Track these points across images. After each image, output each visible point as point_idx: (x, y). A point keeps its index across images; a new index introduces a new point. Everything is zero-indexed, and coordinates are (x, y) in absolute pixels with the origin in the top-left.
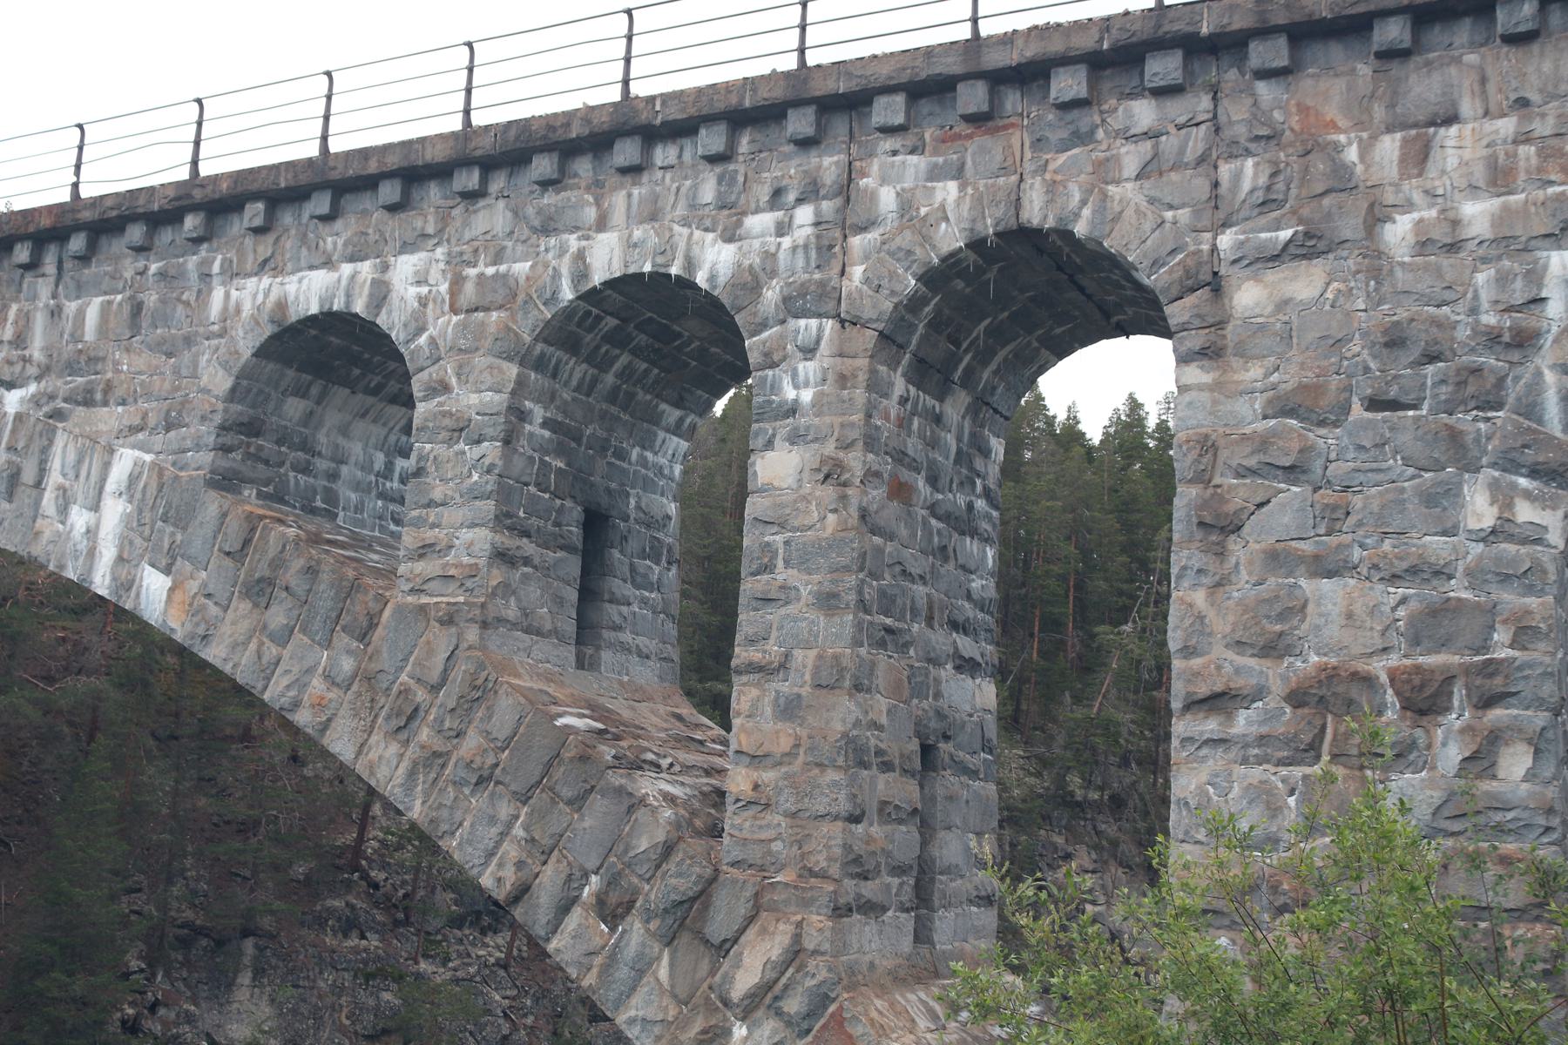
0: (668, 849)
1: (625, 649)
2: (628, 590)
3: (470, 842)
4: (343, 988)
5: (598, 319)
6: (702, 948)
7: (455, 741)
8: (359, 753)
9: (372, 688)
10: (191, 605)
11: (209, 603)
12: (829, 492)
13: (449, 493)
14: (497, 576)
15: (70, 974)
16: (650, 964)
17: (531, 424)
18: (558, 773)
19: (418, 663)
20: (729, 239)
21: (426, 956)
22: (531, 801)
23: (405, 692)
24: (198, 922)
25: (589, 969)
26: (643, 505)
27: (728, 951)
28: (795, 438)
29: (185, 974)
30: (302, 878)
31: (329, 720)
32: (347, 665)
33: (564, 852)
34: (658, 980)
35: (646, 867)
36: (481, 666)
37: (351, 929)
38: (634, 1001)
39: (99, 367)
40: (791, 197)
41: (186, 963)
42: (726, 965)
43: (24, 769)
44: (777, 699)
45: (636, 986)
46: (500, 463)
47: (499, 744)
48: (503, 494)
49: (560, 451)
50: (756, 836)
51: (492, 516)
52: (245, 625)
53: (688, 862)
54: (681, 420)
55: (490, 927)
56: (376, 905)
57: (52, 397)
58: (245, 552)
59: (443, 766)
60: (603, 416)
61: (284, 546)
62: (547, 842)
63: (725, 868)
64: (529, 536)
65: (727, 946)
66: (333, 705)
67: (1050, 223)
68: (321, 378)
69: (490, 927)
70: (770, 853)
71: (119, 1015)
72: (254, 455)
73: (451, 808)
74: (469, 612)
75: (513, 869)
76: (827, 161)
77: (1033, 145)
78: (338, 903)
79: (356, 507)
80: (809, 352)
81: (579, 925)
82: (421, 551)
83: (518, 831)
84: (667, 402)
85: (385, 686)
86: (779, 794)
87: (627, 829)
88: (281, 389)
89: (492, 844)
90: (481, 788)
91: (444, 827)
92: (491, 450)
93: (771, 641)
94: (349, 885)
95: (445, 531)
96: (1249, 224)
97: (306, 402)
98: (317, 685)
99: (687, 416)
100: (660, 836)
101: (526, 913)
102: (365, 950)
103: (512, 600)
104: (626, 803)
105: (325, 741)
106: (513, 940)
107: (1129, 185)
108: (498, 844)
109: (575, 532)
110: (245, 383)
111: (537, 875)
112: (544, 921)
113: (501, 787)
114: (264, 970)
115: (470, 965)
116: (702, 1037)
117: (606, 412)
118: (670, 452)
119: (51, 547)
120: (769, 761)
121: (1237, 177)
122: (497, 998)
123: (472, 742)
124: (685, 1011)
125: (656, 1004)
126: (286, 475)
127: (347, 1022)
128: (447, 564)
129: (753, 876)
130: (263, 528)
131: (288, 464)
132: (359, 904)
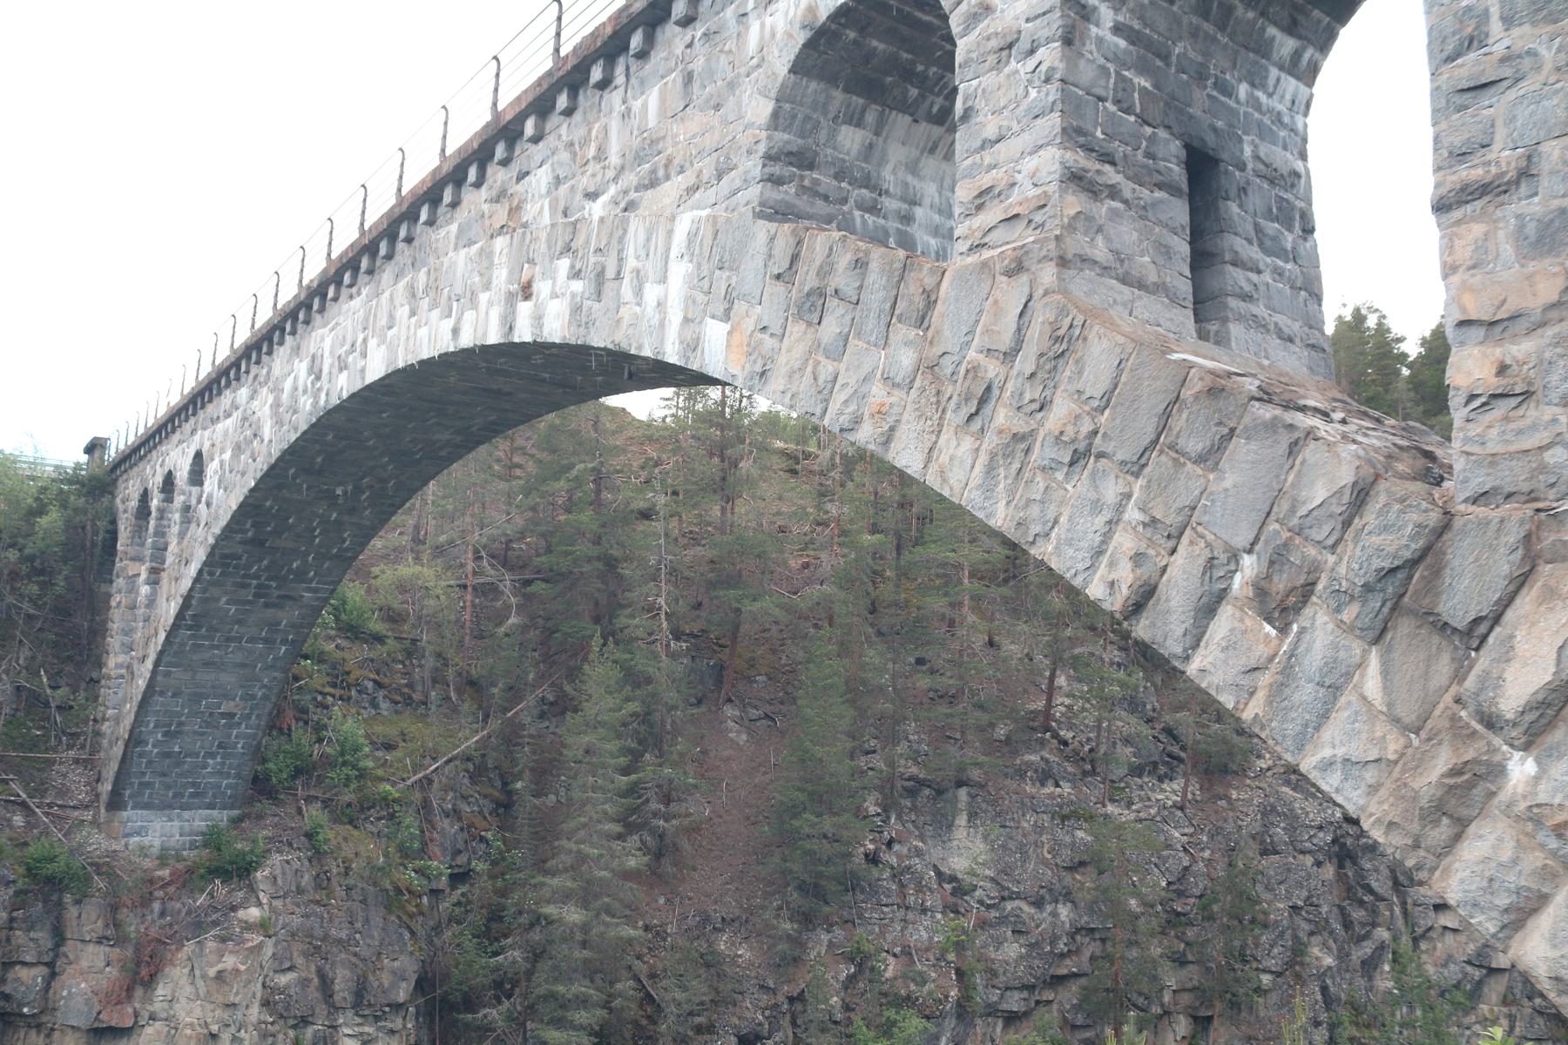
0: (1360, 495)
1: (1262, 326)
2: (1253, 252)
3: (1069, 542)
4: (1043, 828)
6: (1436, 639)
7: (1039, 415)
8: (928, 460)
9: (936, 379)
10: (749, 345)
11: (766, 337)
13: (1005, 123)
14: (1074, 203)
15: (819, 815)
16: (1349, 675)
17: (1097, 25)
18: (1179, 422)
19: (987, 331)
21: (1112, 800)
22: (1147, 470)
23: (974, 370)
24: (921, 776)
25: (1252, 694)
26: (1262, 155)
27: (1484, 638)
29: (913, 817)
30: (1003, 738)
31: (892, 429)
32: (906, 359)
33: (1200, 529)
34: (1364, 698)
35: (1327, 529)
36: (1062, 311)
37: (1046, 779)
38: (1327, 733)
39: (661, 146)
41: (914, 808)
42: (1483, 661)
43: (783, 662)
44: (1521, 228)
45: (1328, 711)
46: (1061, 66)
47: (1096, 403)
48: (1071, 104)
49: (1143, 69)
50: (1513, 448)
51: (1058, 129)
52: (799, 351)
53: (1397, 507)
54: (1297, 55)
55: (1166, 775)
56: (1067, 758)
57: (626, 192)
58: (794, 269)
59: (1027, 451)
60: (1194, 34)
61: (831, 249)
62: (1173, 519)
63: (1462, 507)
64: (1113, 163)
65: (1482, 629)
66: (895, 410)
68: (875, 102)
69: (1166, 775)
70: (1543, 468)
71: (862, 849)
72: (809, 189)
73: (1042, 502)
74: (1041, 249)
75: (1129, 565)
78: (1034, 758)
79: (937, 253)
81: (1232, 630)
82: (978, 201)
83: (1132, 514)
84: (1276, 24)
85: (949, 371)
86: (1547, 372)
87: (1291, 478)
88: (831, 116)
89: (1098, 539)
90: (1077, 468)
91: (1035, 529)
92: (1050, 55)
93: (1496, 147)
94: (1042, 742)
95: (1004, 169)
97: (863, 132)
98: (878, 392)
99: (1304, 49)
100: (1346, 476)
101: (1153, 625)
102: (1060, 796)
103: (1100, 239)
104: (1285, 439)
105: (890, 456)
106: (1186, 785)
108: (1107, 537)
109: (1178, 173)
110: (787, 106)
111: (1164, 570)
112: (1180, 631)
113: (1104, 460)
114: (976, 813)
115: (1150, 807)
116: (1452, 781)
117: (1198, 28)
118: (1288, 97)
119: (630, 331)
120: (1522, 325)
122: (1177, 835)
123: (1061, 409)
124: (1416, 742)
125: (1364, 736)
126: (850, 212)
127: (1049, 856)
128: (1010, 205)
129: (1516, 509)
130: (810, 239)
131: (851, 202)
132: (1052, 758)
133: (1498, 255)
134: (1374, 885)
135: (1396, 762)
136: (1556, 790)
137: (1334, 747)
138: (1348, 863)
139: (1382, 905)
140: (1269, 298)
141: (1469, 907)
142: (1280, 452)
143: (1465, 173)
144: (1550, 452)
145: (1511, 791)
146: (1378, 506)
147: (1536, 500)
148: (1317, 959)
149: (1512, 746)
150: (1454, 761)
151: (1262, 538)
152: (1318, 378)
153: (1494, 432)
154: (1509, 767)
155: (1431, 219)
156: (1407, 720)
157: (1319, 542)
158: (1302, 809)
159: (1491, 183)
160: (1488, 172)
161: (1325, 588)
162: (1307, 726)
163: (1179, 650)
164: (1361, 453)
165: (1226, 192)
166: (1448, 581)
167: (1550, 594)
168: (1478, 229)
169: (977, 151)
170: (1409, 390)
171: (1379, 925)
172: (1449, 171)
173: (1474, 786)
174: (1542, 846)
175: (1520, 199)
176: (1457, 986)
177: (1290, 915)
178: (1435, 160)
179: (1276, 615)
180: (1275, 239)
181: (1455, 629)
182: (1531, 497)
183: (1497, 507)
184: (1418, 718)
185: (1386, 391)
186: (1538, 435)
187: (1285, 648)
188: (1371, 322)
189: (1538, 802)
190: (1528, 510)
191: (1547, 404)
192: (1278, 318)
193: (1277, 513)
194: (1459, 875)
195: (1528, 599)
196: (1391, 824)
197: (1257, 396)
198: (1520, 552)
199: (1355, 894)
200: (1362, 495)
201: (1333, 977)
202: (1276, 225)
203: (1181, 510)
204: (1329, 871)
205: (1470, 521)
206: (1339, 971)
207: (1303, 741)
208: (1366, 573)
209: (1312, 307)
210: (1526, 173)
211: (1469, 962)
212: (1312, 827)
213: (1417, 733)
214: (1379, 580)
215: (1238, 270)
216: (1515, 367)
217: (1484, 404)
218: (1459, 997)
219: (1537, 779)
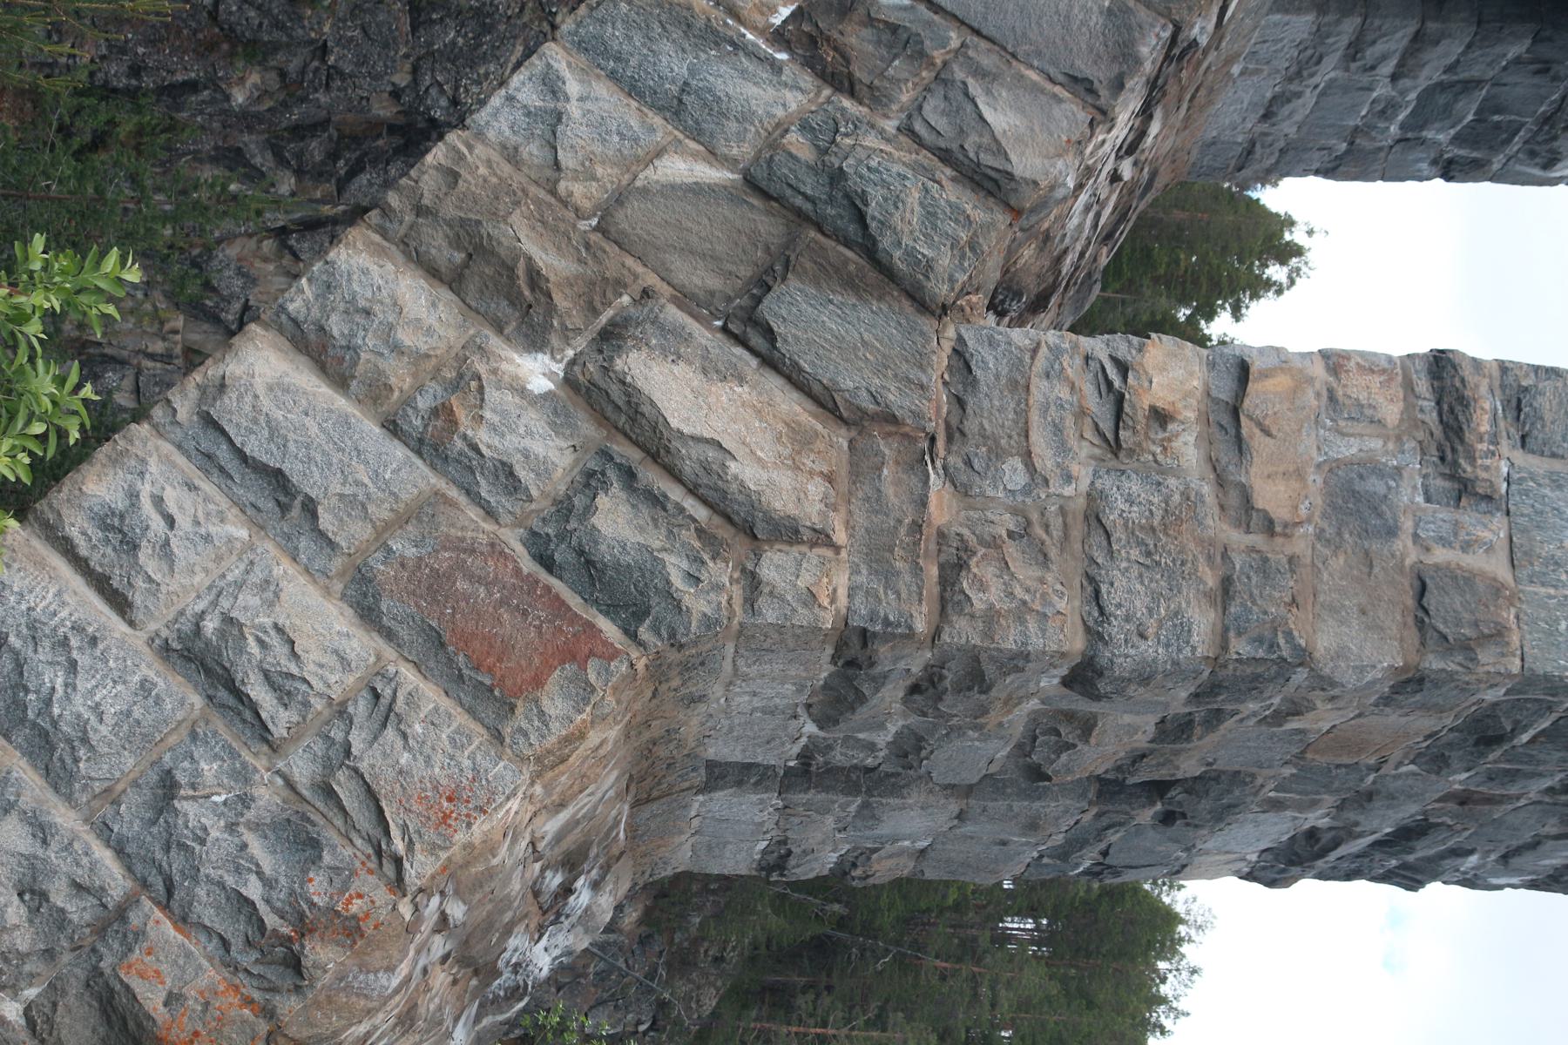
1: (1298, 73)
2: (1431, 72)
6: (746, 272)
16: (696, 134)
27: (742, 341)
34: (659, 154)
35: (941, 123)
38: (603, 90)
42: (704, 336)
44: (1379, 471)
50: (1035, 417)
53: (964, 236)
63: (951, 332)
65: (757, 340)
70: (997, 454)
87: (1033, 75)
93: (1519, 457)
100: (1024, 163)
104: (1100, 74)
120: (1226, 455)
124: (583, 225)
125: (598, 148)
129: (938, 409)
133: (1344, 435)
134: (364, 178)
135: (553, 192)
136: (504, 414)
137: (581, 99)
138: (397, 141)
139: (331, 187)
140: (1346, 90)
141: (324, 277)
142: (1078, 63)
143: (1487, 406)
144: (1020, 466)
145: (503, 353)
146: (968, 208)
147: (950, 439)
148: (242, 80)
149: (573, 362)
150: (552, 278)
151: (936, 18)
152: (1195, 152)
153: (1063, 393)
154: (540, 356)
155: (1423, 345)
156: (620, 215)
157: (920, 108)
158: (487, 75)
159: (1462, 441)
160: (1481, 440)
161: (843, 110)
162: (618, 59)
164: (1060, 193)
165: (1550, 39)
166: (837, 299)
167: (801, 440)
168: (1391, 412)
170: (1153, 314)
171: (299, 180)
172: (1497, 383)
173: (512, 304)
174: (420, 389)
175: (1425, 477)
176: (207, 286)
177: (312, 42)
178: (1520, 365)
179: (806, 28)
180: (1446, 112)
181: (758, 300)
182: (955, 433)
183: (945, 383)
184: (623, 232)
185: (1156, 280)
186: (1049, 453)
187: (749, 36)
188: (1276, 272)
189: (487, 390)
190: (936, 426)
191: (1095, 472)
192: (1309, 99)
193: (976, 47)
194: (374, 268)
195: (798, 409)
196: (453, 177)
197: (1181, 37)
198: (872, 407)
199: (348, 148)
200: (989, 185)
201: (213, 101)
202: (1470, 117)
204: (383, 109)
205: (928, 341)
206: (224, 112)
207: (594, 52)
208: (861, 177)
209: (1317, 159)
210: (1464, 490)
212: (457, 88)
213: (597, 229)
214: (847, 196)
215: (1405, 42)
216: (1161, 435)
217: (1109, 384)
218: (193, 289)
219: (522, 391)
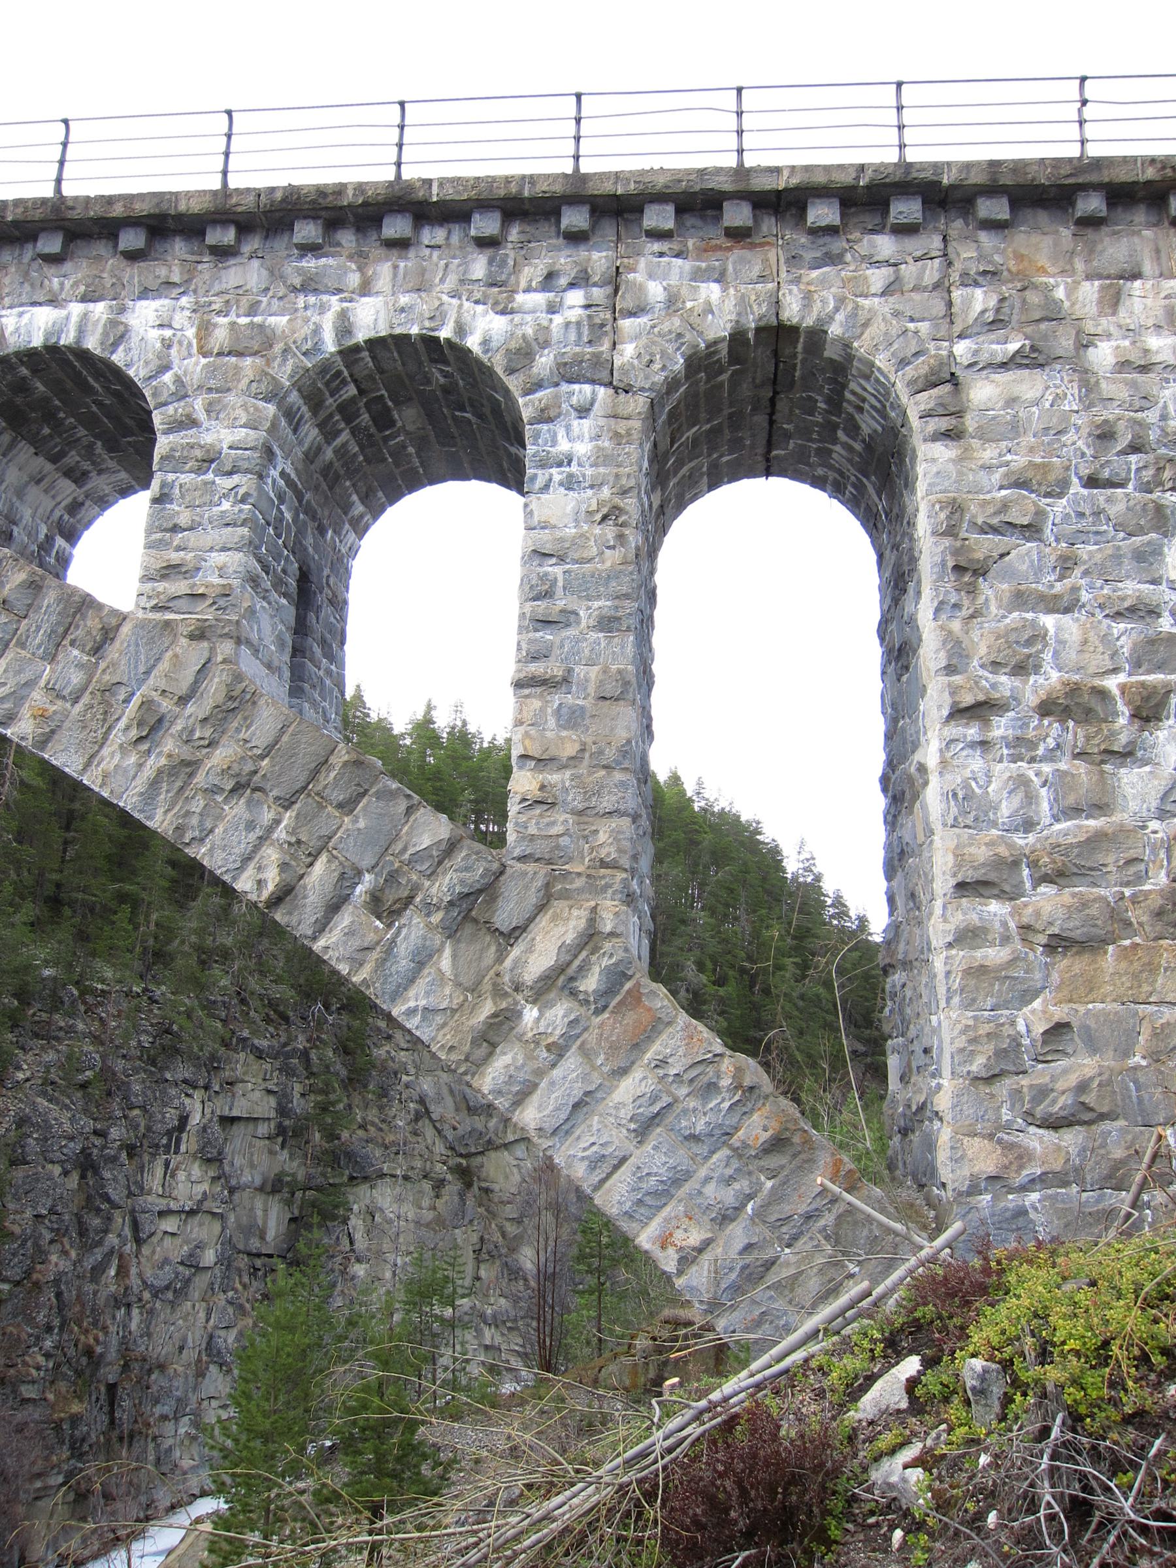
5: (344, 383)
7: (205, 751)
12: (609, 532)
16: (431, 956)
20: (503, 312)
25: (361, 965)
28: (570, 484)
31: (53, 732)
38: (411, 993)
40: (563, 281)
42: (515, 952)
59: (191, 775)
65: (517, 933)
67: (809, 322)
70: (557, 847)
75: (276, 871)
76: (595, 255)
77: (787, 261)
80: (583, 411)
89: (250, 847)
96: (981, 338)
107: (876, 300)
108: (256, 848)
111: (302, 877)
121: (968, 302)
155: (510, 691)
163: (309, 932)
167: (554, 918)
168: (536, 704)
169: (166, 530)
176: (167, 1288)
196: (452, 1048)
203: (321, 837)
204: (73, 1181)
210: (566, 680)
211: (182, 1263)
219: (538, 1020)
